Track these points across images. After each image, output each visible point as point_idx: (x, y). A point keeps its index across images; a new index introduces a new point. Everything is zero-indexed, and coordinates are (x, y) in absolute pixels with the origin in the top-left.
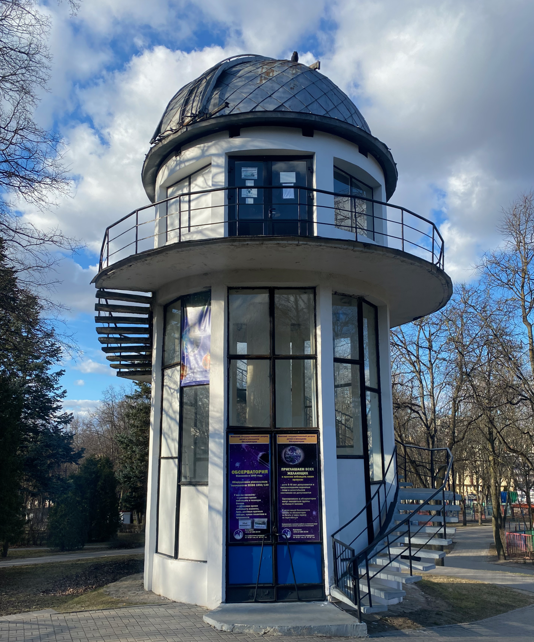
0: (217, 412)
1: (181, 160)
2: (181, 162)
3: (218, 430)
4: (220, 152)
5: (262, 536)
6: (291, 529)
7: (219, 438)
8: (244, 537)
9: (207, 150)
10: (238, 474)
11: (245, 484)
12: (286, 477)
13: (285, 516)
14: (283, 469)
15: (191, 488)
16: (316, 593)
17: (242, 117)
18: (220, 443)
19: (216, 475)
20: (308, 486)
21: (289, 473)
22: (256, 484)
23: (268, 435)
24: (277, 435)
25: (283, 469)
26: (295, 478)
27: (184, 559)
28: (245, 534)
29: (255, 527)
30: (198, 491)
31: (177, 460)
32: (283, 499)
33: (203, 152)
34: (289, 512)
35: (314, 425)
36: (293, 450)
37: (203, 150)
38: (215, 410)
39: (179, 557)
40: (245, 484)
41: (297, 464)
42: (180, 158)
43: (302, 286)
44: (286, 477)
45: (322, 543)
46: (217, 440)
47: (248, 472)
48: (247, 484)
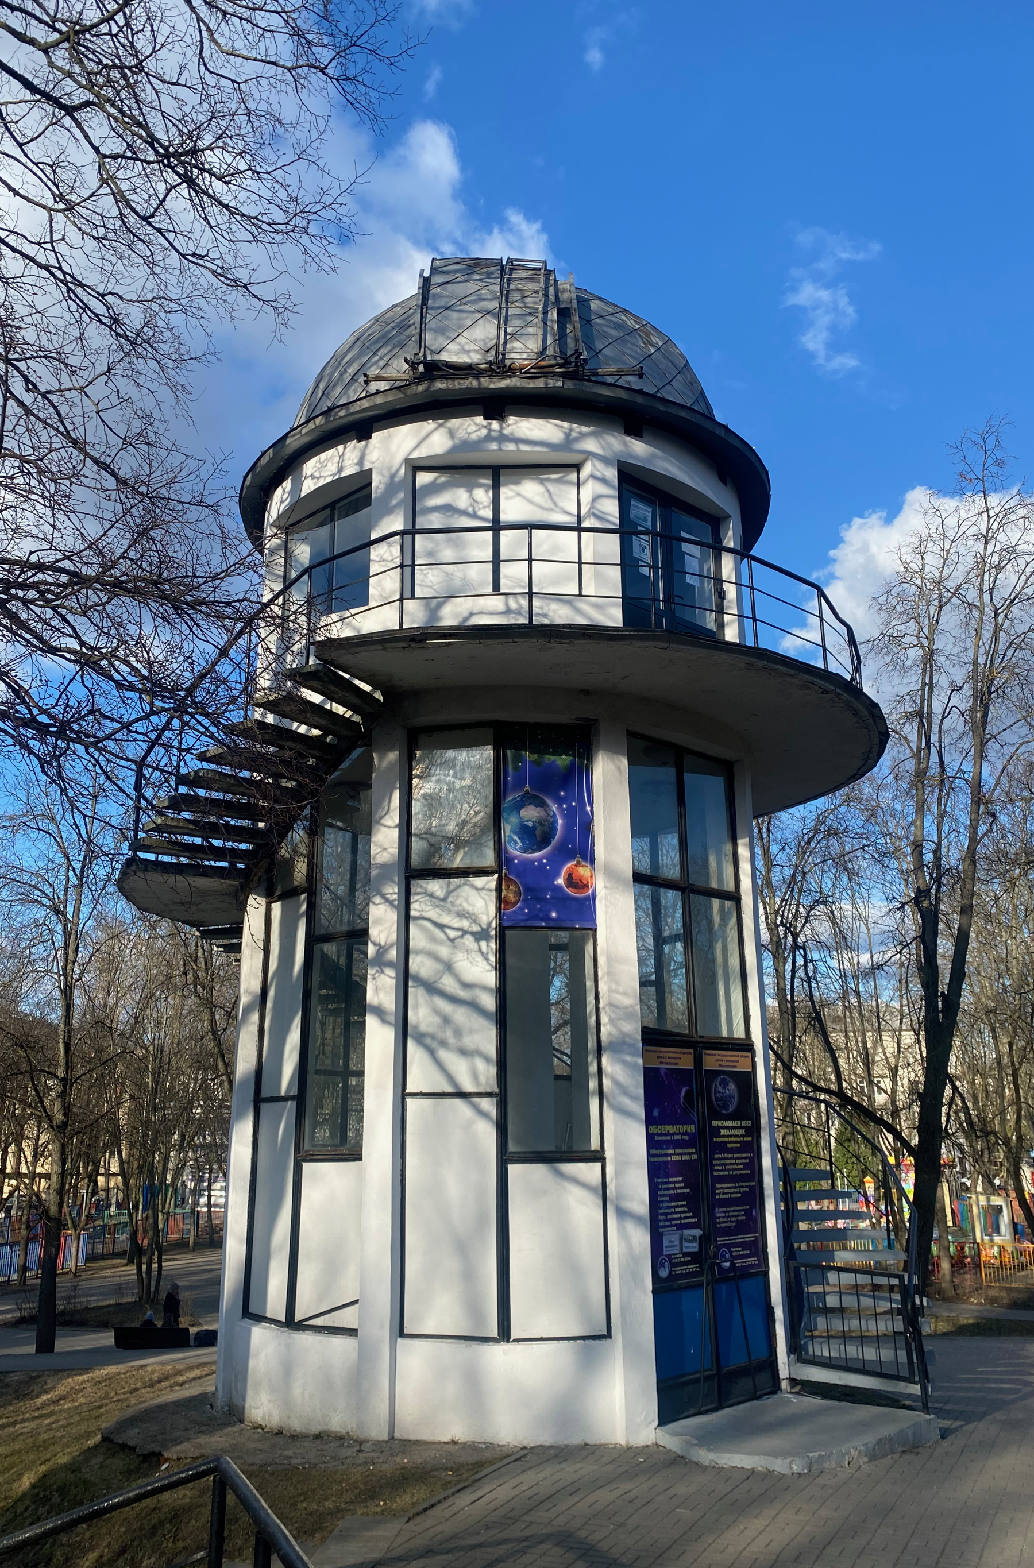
0: (625, 994)
1: (506, 432)
2: (502, 438)
3: (629, 1036)
4: (608, 454)
5: (693, 1268)
6: (729, 1246)
7: (633, 1054)
8: (671, 1271)
9: (576, 439)
10: (658, 1134)
11: (667, 1155)
12: (718, 1140)
13: (720, 1223)
14: (715, 1123)
15: (539, 1170)
16: (764, 1377)
17: (673, 410)
18: (636, 1065)
19: (623, 1136)
20: (745, 1158)
21: (722, 1132)
22: (681, 1154)
23: (692, 1051)
24: (704, 1051)
25: (715, 1123)
26: (732, 1142)
27: (542, 1339)
28: (673, 1265)
29: (684, 1250)
30: (560, 1174)
31: (489, 1106)
32: (718, 1186)
33: (568, 441)
34: (725, 1212)
35: (739, 1033)
36: (724, 1084)
37: (568, 435)
38: (621, 989)
39: (514, 1335)
40: (667, 1155)
41: (730, 1114)
42: (502, 428)
43: (700, 749)
44: (718, 1140)
45: (766, 1274)
46: (628, 1058)
47: (670, 1129)
48: (671, 1155)
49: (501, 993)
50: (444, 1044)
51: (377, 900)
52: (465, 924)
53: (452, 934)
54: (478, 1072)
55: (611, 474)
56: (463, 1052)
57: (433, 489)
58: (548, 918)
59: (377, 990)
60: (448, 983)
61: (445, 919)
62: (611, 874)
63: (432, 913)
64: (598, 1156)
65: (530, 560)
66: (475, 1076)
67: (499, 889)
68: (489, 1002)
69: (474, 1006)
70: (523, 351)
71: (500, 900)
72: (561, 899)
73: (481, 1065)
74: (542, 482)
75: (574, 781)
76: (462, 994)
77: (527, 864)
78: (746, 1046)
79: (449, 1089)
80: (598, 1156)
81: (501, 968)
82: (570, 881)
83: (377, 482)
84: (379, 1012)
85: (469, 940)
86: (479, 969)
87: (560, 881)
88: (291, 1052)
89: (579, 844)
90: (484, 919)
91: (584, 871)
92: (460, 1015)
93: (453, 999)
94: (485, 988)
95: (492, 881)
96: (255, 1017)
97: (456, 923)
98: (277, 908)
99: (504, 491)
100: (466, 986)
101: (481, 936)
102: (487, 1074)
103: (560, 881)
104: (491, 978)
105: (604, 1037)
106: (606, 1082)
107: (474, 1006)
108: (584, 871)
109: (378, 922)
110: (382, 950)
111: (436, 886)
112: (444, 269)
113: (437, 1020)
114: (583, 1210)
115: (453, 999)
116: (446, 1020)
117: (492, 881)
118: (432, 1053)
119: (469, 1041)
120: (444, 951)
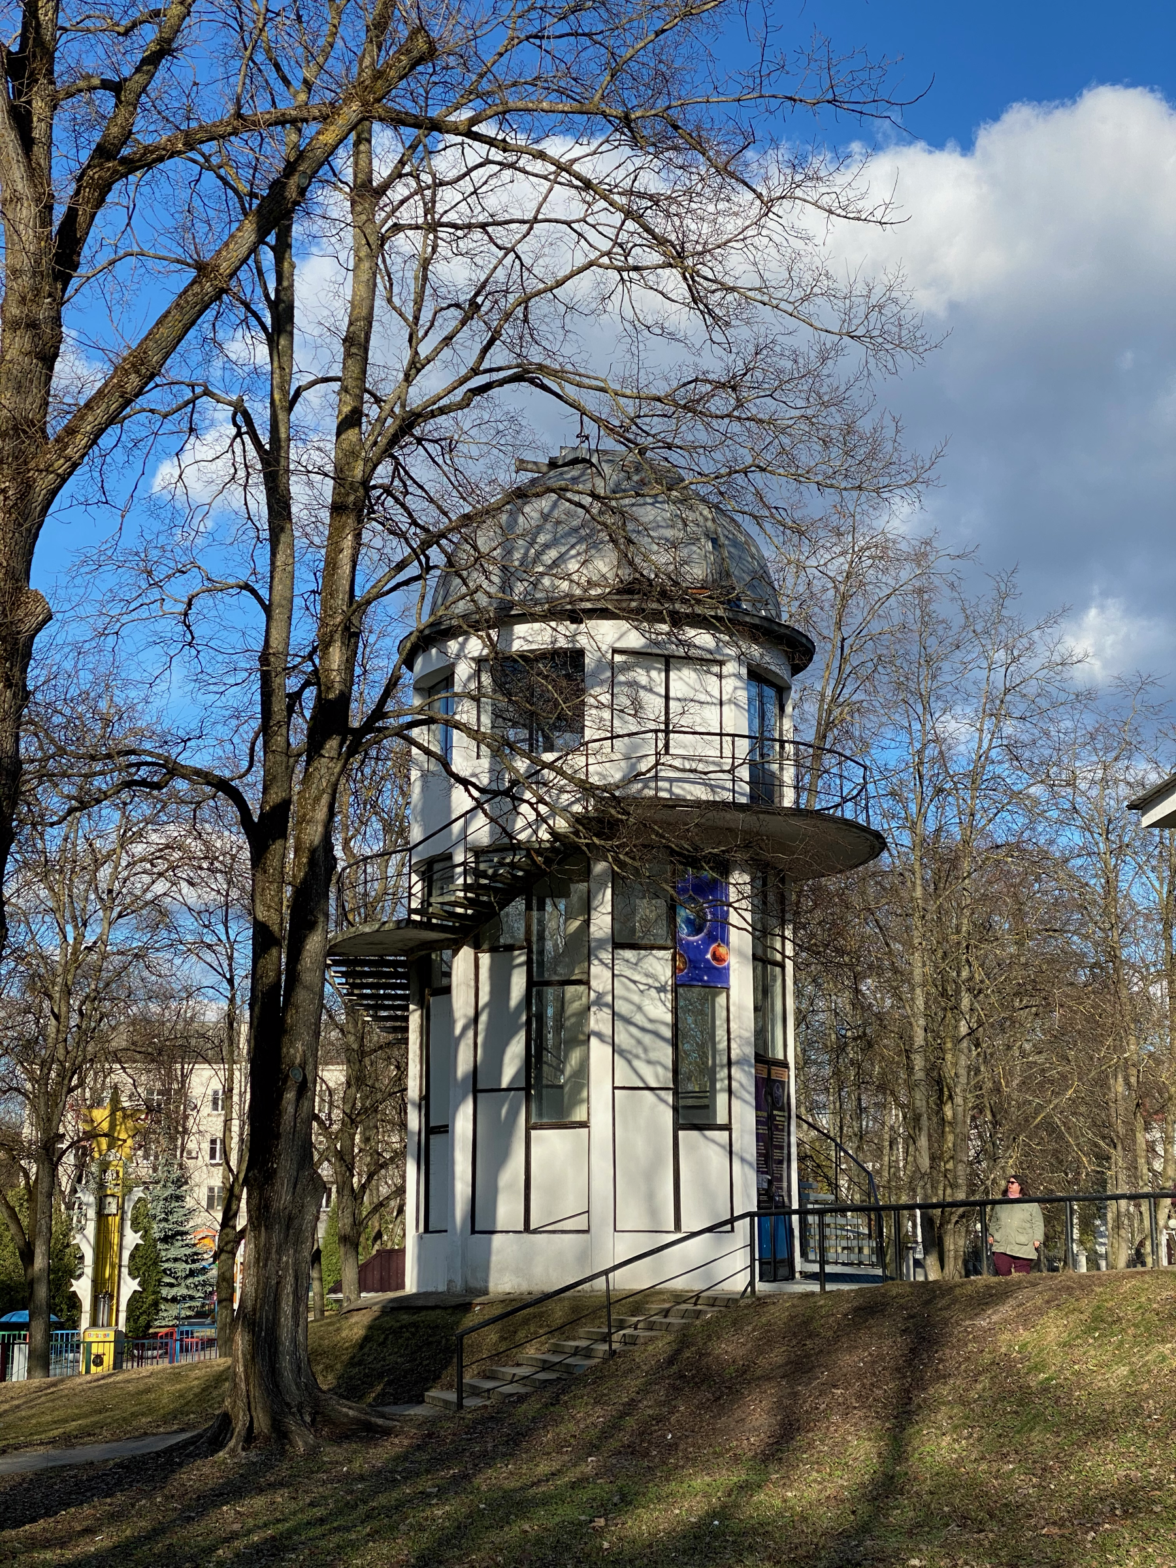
19: (744, 1117)
35: (780, 1056)
49: (675, 1026)
50: (637, 1057)
51: (596, 962)
52: (650, 981)
53: (642, 987)
54: (658, 1074)
55: (744, 671)
56: (649, 1062)
57: (625, 668)
58: (702, 980)
59: (597, 1021)
60: (639, 1019)
61: (636, 978)
62: (741, 954)
63: (628, 973)
64: (727, 1127)
65: (721, 735)
66: (657, 1076)
67: (674, 959)
68: (668, 1033)
69: (656, 1034)
70: (697, 572)
71: (674, 967)
72: (710, 969)
73: (660, 1070)
74: (695, 670)
75: (711, 891)
76: (649, 1026)
77: (689, 943)
78: (785, 1065)
79: (641, 1085)
80: (727, 1127)
81: (675, 1011)
82: (715, 957)
83: (589, 661)
84: (599, 1035)
85: (653, 992)
86: (660, 1010)
87: (709, 956)
88: (512, 1059)
89: (719, 933)
90: (663, 979)
91: (722, 950)
92: (647, 1039)
93: (643, 1029)
94: (666, 1024)
95: (667, 954)
96: (471, 1033)
97: (644, 980)
98: (485, 959)
99: (672, 674)
100: (651, 1021)
101: (661, 989)
102: (666, 1078)
103: (709, 956)
104: (669, 1018)
105: (733, 1056)
106: (734, 1084)
107: (656, 1034)
108: (722, 950)
109: (596, 977)
110: (600, 996)
111: (629, 954)
112: (265, 439)
113: (633, 1042)
114: (716, 1158)
115: (643, 1029)
116: (639, 1042)
117: (667, 954)
118: (629, 1062)
119: (653, 1056)
120: (636, 998)
